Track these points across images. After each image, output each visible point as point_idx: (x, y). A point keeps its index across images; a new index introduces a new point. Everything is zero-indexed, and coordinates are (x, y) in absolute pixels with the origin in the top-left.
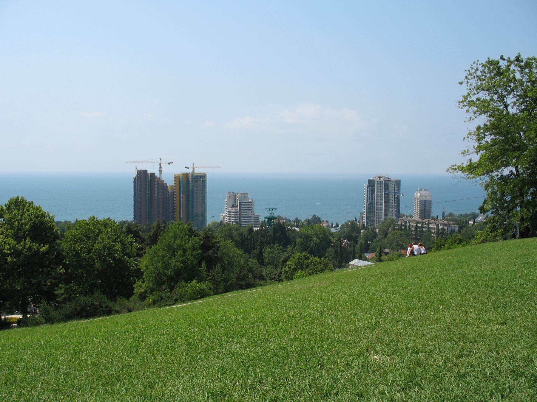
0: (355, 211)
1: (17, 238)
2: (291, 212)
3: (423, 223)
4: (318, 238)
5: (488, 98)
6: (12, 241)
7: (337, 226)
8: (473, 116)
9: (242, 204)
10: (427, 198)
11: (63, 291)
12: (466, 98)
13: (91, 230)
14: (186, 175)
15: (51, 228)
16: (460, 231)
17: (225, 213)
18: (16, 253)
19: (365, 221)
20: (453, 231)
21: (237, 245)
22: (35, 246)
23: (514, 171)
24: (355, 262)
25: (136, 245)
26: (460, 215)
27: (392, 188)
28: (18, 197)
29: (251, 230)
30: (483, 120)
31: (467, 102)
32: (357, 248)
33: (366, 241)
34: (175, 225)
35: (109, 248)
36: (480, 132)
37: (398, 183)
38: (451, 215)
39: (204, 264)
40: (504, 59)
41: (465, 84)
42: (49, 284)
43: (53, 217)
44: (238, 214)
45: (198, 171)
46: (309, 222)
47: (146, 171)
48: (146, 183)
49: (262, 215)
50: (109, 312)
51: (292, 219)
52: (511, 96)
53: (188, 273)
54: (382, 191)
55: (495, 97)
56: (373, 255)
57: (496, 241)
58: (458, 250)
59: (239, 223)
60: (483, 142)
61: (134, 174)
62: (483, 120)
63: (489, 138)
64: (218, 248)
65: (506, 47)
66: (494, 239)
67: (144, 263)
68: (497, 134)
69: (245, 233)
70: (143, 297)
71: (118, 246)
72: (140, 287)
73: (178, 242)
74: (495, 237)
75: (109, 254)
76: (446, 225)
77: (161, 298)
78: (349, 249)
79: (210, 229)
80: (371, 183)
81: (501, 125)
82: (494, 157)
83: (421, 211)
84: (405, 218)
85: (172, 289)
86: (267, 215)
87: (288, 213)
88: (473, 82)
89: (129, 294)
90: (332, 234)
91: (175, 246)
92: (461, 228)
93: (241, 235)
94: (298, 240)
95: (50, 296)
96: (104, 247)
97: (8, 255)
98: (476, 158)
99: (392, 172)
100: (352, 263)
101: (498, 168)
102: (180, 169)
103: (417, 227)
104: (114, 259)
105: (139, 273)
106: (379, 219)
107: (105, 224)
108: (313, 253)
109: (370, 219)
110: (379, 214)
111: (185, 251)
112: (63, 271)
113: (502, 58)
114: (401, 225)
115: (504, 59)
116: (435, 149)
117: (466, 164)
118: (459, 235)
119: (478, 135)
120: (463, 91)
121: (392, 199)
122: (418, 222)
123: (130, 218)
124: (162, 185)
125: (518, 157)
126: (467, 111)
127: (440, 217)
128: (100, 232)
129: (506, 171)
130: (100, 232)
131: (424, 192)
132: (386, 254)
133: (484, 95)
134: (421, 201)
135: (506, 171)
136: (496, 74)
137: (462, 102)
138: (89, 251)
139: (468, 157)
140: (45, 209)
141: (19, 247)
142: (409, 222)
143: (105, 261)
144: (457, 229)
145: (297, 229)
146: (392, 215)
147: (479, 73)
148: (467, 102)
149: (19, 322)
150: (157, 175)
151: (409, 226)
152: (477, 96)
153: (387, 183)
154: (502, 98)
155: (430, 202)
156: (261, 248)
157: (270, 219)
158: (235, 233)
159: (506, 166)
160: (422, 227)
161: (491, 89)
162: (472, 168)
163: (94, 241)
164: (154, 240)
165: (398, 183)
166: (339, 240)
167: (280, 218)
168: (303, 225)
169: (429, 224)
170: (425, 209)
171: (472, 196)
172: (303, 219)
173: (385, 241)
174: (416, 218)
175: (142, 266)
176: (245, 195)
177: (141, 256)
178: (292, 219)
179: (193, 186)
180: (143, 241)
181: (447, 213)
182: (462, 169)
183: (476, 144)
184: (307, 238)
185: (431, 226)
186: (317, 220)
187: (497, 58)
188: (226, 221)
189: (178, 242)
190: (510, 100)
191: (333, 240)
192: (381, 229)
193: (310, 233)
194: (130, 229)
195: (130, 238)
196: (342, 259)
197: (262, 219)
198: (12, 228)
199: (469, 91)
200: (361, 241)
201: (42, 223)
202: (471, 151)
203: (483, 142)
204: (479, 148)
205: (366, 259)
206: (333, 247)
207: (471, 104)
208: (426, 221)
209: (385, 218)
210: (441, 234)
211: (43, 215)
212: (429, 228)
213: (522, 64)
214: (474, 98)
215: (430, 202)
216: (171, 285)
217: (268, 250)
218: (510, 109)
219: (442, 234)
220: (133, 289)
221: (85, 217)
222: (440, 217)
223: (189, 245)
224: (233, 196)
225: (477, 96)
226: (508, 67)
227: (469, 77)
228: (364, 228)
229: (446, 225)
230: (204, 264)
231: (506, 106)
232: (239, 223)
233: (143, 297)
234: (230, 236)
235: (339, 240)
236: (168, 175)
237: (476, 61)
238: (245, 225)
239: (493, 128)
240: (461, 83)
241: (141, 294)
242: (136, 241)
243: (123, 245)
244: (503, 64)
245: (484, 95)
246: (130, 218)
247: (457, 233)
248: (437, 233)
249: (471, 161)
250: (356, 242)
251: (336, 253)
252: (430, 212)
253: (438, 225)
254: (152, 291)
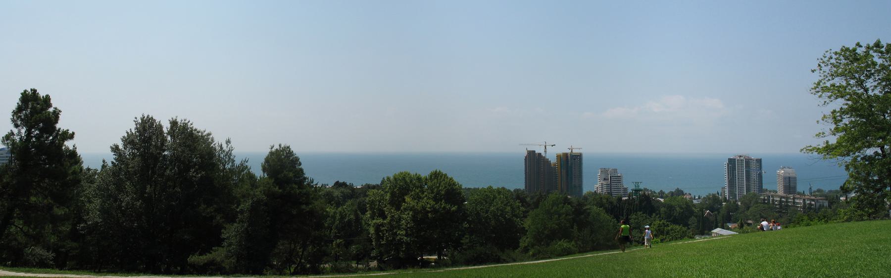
0: (717, 185)
1: (436, 199)
2: (657, 185)
3: (787, 198)
4: (681, 208)
5: (844, 84)
6: (432, 203)
7: (699, 198)
8: (828, 100)
9: (612, 178)
10: (791, 175)
11: (467, 241)
12: (819, 84)
13: (489, 196)
14: (566, 155)
15: (460, 193)
16: (830, 207)
17: (598, 185)
18: (434, 211)
19: (727, 194)
20: (821, 207)
21: (607, 211)
22: (448, 207)
23: (880, 152)
24: (718, 230)
25: (524, 209)
26: (830, 191)
27: (753, 166)
28: (115, 149)
29: (620, 199)
30: (840, 104)
31: (819, 88)
32: (719, 218)
33: (729, 212)
34: (554, 196)
35: (501, 210)
36: (836, 117)
38: (819, 191)
39: (575, 227)
40: (861, 46)
41: (818, 71)
42: (47, 181)
43: (56, 114)
44: (610, 186)
45: (575, 151)
46: (672, 194)
48: (534, 160)
49: (630, 188)
50: (498, 261)
51: (657, 191)
52: (871, 80)
53: (562, 233)
54: (743, 168)
55: (852, 82)
56: (736, 225)
57: (863, 220)
58: (818, 227)
59: (610, 193)
60: (841, 125)
61: (525, 153)
62: (840, 104)
63: (846, 120)
64: (589, 214)
65: (861, 36)
66: (861, 218)
67: (527, 223)
68: (857, 116)
69: (615, 202)
70: (526, 250)
71: (509, 208)
72: (524, 242)
73: (555, 208)
74: (861, 216)
75: (501, 215)
76: (813, 200)
77: (539, 252)
78: (712, 219)
79: (586, 198)
80: (732, 162)
81: (861, 108)
82: (851, 141)
83: (785, 187)
84: (768, 193)
85: (548, 245)
86: (634, 188)
87: (652, 185)
88: (827, 69)
89: (516, 247)
90: (694, 206)
91: (552, 211)
92: (831, 203)
93: (611, 203)
94: (662, 209)
95: (457, 244)
96: (497, 209)
97: (428, 212)
98: (833, 140)
99: (753, 150)
100: (715, 231)
101: (859, 149)
102: (563, 149)
103: (781, 201)
104: (505, 218)
105: (524, 231)
106: (742, 191)
107: (499, 191)
108: (675, 221)
109: (731, 192)
110: (741, 189)
111: (560, 215)
112: (467, 226)
113: (858, 45)
114: (764, 200)
115: (861, 46)
116: (787, 125)
117: (822, 145)
118: (829, 210)
119: (834, 118)
120: (816, 77)
121: (754, 175)
122: (781, 197)
123: (522, 186)
124: (546, 162)
125: (884, 138)
126: (820, 97)
127: (807, 193)
128: (495, 198)
129: (870, 152)
130: (495, 198)
131: (790, 170)
132: (749, 225)
133: (839, 81)
134: (785, 178)
135: (870, 152)
136: (853, 62)
137: (815, 88)
138: (487, 212)
139: (825, 139)
140: (456, 180)
141: (437, 206)
142: (772, 196)
144: (826, 204)
145: (662, 200)
146: (754, 189)
147: (833, 61)
148: (819, 88)
149: (435, 261)
150: (543, 154)
151: (773, 200)
152: (832, 82)
153: (748, 161)
154: (860, 83)
155: (795, 178)
156: (628, 215)
157: (637, 191)
158: (605, 201)
159: (869, 147)
160: (787, 202)
161: (848, 74)
162: (829, 149)
163: (490, 204)
164: (536, 205)
165: (759, 161)
166: (702, 210)
167: (646, 190)
168: (667, 196)
169: (794, 199)
170: (790, 185)
171: (834, 174)
172: (667, 192)
173: (748, 213)
174: (781, 192)
175: (526, 226)
176: (615, 170)
177: (526, 217)
178: (657, 191)
179: (571, 163)
180: (529, 205)
181: (814, 189)
182: (818, 150)
183: (833, 126)
184: (670, 208)
185: (797, 201)
186: (680, 192)
187: (852, 46)
188: (599, 191)
189: (555, 208)
190: (870, 83)
191: (696, 210)
192: (744, 201)
193: (673, 203)
194: (518, 196)
195: (518, 203)
196: (705, 228)
197: (629, 191)
198: (432, 193)
199: (820, 78)
200: (723, 212)
201: (453, 190)
202: (827, 134)
203: (841, 125)
204: (837, 130)
205: (728, 229)
206: (696, 217)
207: (825, 89)
208: (791, 196)
209: (748, 190)
210: (808, 209)
211: (454, 184)
212: (794, 202)
213: (883, 49)
214: (828, 84)
215: (795, 178)
216: (547, 242)
217: (634, 216)
218: (870, 93)
219: (810, 208)
220: (519, 243)
221: (485, 185)
222: (807, 193)
223: (564, 210)
224: (604, 171)
225: (832, 82)
226: (867, 54)
227: (822, 65)
228: (725, 200)
229: (813, 200)
230: (575, 227)
231: (866, 90)
232: (610, 193)
233: (526, 250)
234: (600, 205)
235: (702, 210)
236: (551, 155)
237: (818, 62)
238: (615, 195)
239: (852, 110)
240: (813, 71)
241: (525, 247)
242: (523, 206)
243: (512, 208)
244: (860, 51)
245: (839, 81)
246: (522, 186)
247: (823, 210)
248: (804, 207)
249: (827, 142)
250: (719, 212)
251: (699, 221)
252: (795, 188)
253: (804, 200)
254: (533, 246)
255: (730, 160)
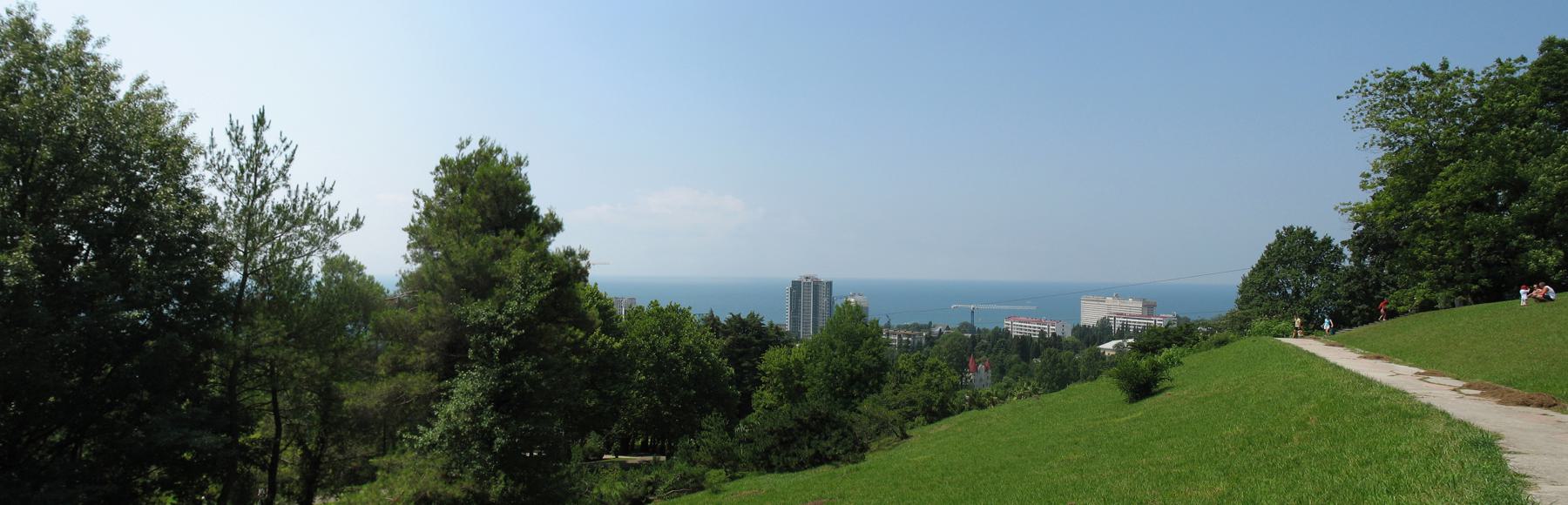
27: (823, 291)
37: (830, 284)
47: (445, 163)
143: (698, 363)
153: (817, 285)
165: (830, 284)
255: (794, 283)
